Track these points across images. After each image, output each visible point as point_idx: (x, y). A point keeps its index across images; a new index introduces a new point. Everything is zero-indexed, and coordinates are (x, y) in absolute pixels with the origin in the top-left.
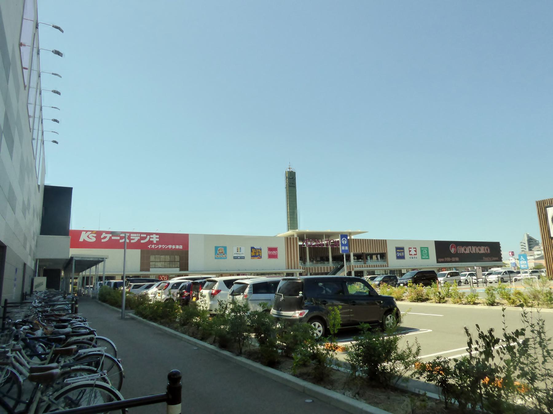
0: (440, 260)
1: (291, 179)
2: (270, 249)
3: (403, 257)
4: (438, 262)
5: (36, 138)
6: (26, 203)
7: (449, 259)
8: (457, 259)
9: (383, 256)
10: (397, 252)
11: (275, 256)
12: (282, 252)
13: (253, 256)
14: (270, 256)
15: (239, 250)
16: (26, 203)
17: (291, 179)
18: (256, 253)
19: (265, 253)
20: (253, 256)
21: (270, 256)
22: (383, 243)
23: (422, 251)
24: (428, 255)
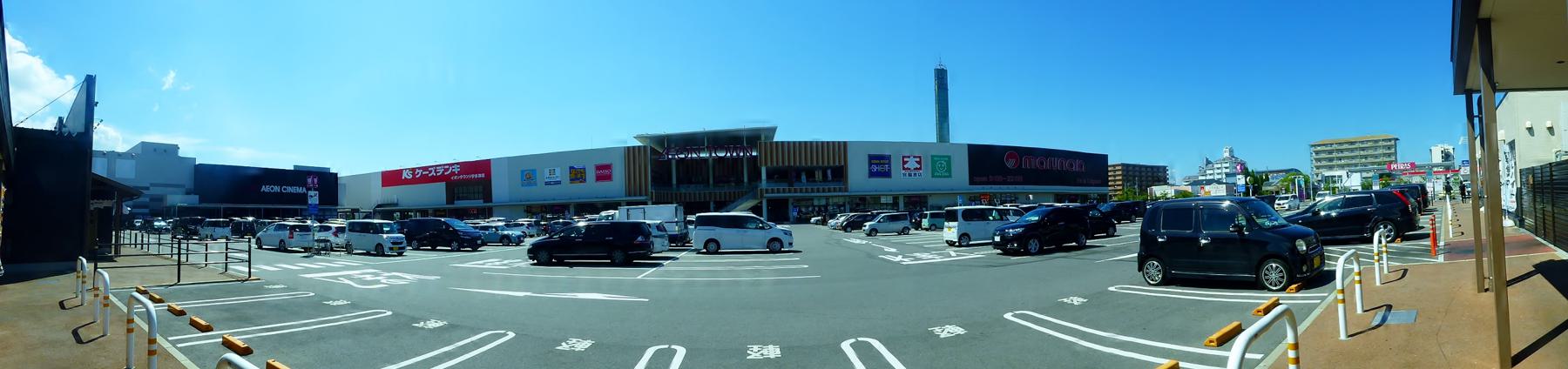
0: (977, 179)
1: (941, 76)
2: (599, 168)
3: (887, 174)
4: (972, 182)
5: (1167, 362)
6: (226, 315)
7: (1000, 178)
8: (1020, 178)
9: (840, 173)
10: (870, 164)
11: (609, 178)
12: (619, 173)
13: (572, 180)
14: (599, 178)
15: (552, 172)
16: (226, 315)
17: (941, 76)
18: (577, 175)
19: (591, 174)
20: (572, 180)
21: (599, 178)
22: (842, 147)
23: (934, 163)
24: (949, 170)
